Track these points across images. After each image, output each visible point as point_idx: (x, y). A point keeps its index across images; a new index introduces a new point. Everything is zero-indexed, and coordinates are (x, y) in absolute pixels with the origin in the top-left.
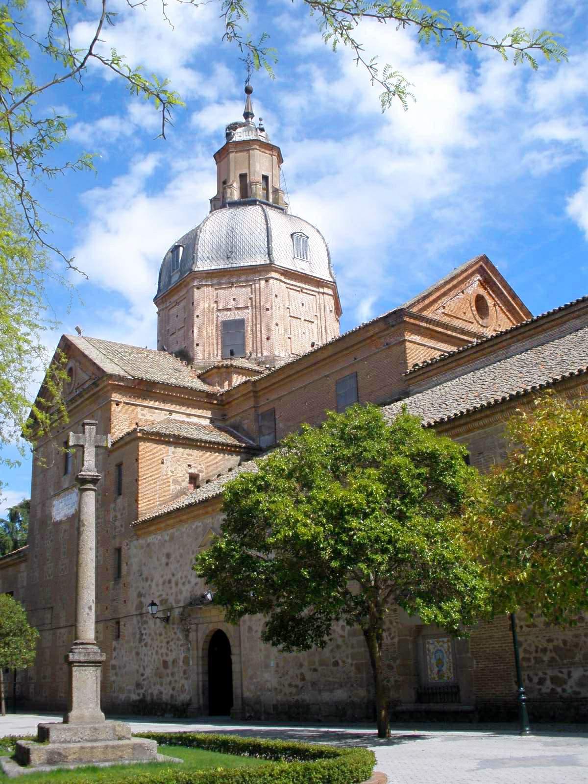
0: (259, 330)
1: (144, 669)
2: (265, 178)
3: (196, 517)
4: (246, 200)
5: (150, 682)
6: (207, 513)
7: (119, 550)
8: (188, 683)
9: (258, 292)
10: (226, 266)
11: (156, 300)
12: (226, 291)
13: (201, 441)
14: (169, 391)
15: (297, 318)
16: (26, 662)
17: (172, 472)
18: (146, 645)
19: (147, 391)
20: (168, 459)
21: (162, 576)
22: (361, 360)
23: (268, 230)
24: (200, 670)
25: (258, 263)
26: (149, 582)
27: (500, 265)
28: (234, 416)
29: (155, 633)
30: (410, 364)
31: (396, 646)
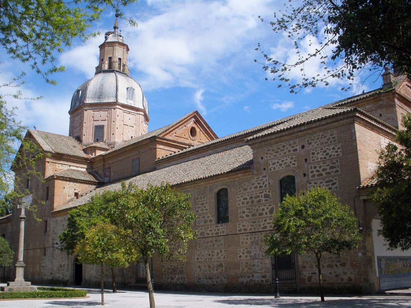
4: (111, 70)
9: (110, 114)
10: (98, 102)
11: (70, 112)
12: (97, 113)
13: (80, 180)
14: (69, 157)
16: (9, 263)
17: (68, 192)
18: (55, 259)
27: (204, 114)
30: (158, 157)
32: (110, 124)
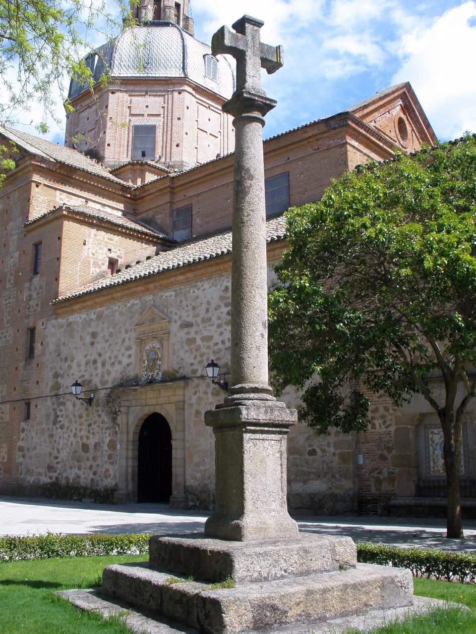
0: (169, 136)
1: (59, 452)
2: (178, 6)
3: (133, 295)
4: (159, 21)
5: (65, 465)
6: (147, 290)
7: (32, 331)
8: (118, 466)
9: (170, 102)
12: (140, 98)
15: (204, 131)
17: (93, 254)
18: (62, 427)
19: (67, 176)
20: (90, 241)
21: (85, 356)
22: (294, 160)
23: (183, 45)
24: (130, 454)
25: (174, 76)
26: (69, 363)
28: (146, 211)
29: (74, 415)
31: (392, 435)
32: (169, 124)
